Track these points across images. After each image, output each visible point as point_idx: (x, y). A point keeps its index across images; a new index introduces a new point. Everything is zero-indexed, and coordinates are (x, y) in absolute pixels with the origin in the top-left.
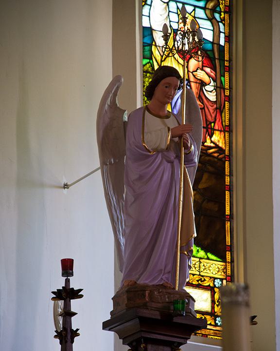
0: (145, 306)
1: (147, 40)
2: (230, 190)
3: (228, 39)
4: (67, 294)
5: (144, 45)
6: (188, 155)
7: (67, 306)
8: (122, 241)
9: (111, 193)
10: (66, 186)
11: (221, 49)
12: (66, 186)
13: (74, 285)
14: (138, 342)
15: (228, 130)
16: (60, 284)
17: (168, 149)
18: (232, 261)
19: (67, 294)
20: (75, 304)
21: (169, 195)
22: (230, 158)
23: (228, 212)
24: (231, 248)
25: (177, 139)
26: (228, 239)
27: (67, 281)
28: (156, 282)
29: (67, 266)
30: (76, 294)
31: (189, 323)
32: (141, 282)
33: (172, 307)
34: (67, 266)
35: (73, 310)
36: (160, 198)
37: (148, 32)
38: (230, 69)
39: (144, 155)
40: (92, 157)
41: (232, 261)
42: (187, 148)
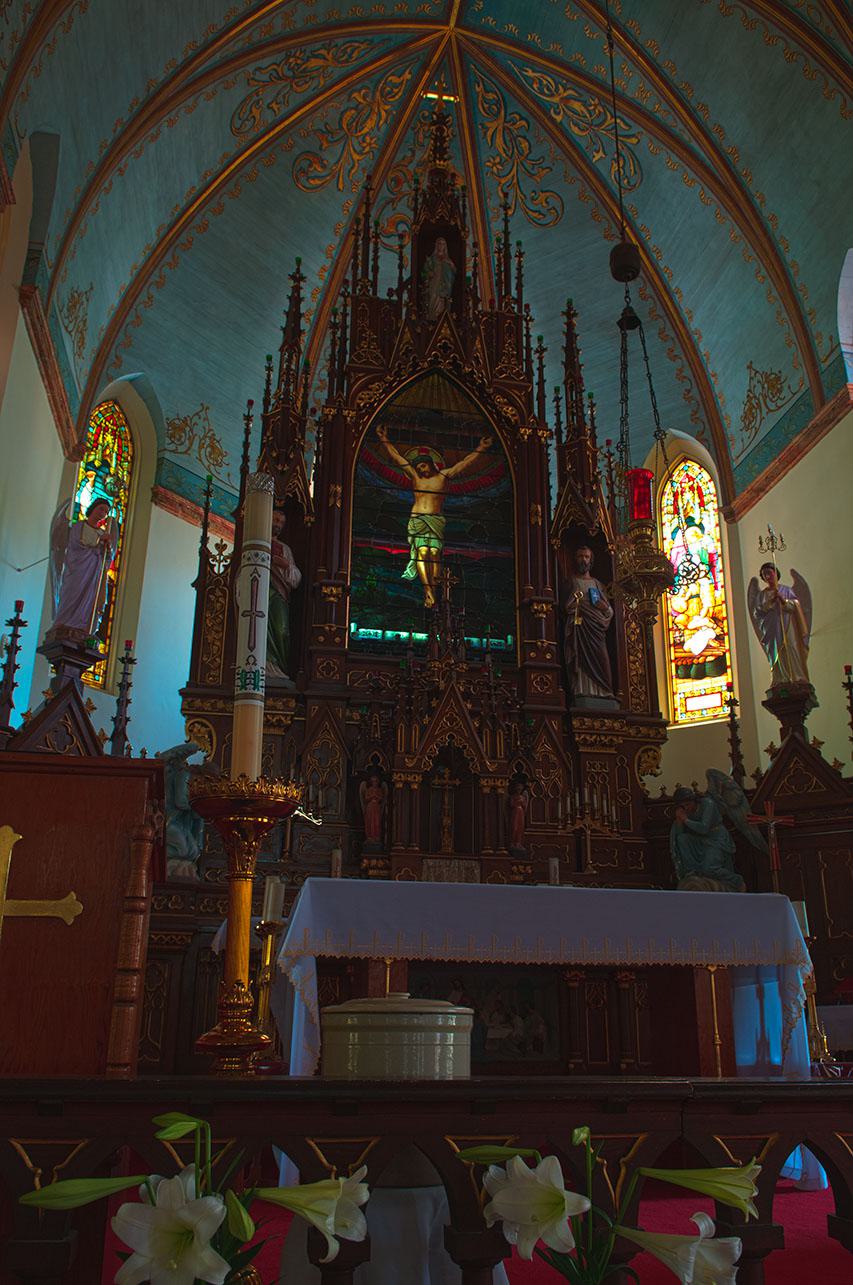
0: (68, 639)
1: (77, 509)
2: (114, 605)
3: (124, 521)
4: (16, 623)
5: (75, 512)
6: (109, 553)
7: (15, 630)
8: (57, 601)
9: (54, 568)
10: (19, 570)
11: (120, 525)
12: (19, 570)
13: (22, 617)
14: (59, 662)
15: (117, 570)
16: (13, 615)
17: (96, 547)
18: (110, 645)
19: (16, 623)
20: (21, 630)
21: (93, 575)
22: (116, 586)
23: (111, 616)
24: (110, 638)
25: (102, 543)
26: (109, 632)
27: (18, 615)
28: (77, 626)
29: (19, 606)
30: (23, 624)
31: (94, 654)
32: (68, 624)
33: (86, 643)
34: (19, 606)
35: (19, 633)
36: (87, 576)
37: (78, 506)
38: (123, 537)
39: (80, 548)
40: (44, 550)
41: (110, 645)
42: (109, 549)
